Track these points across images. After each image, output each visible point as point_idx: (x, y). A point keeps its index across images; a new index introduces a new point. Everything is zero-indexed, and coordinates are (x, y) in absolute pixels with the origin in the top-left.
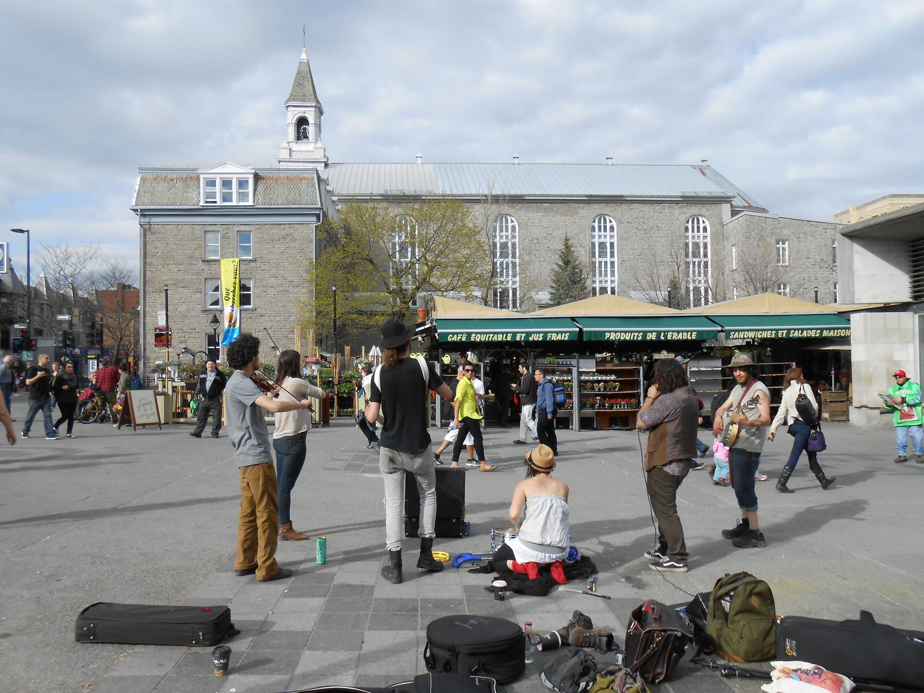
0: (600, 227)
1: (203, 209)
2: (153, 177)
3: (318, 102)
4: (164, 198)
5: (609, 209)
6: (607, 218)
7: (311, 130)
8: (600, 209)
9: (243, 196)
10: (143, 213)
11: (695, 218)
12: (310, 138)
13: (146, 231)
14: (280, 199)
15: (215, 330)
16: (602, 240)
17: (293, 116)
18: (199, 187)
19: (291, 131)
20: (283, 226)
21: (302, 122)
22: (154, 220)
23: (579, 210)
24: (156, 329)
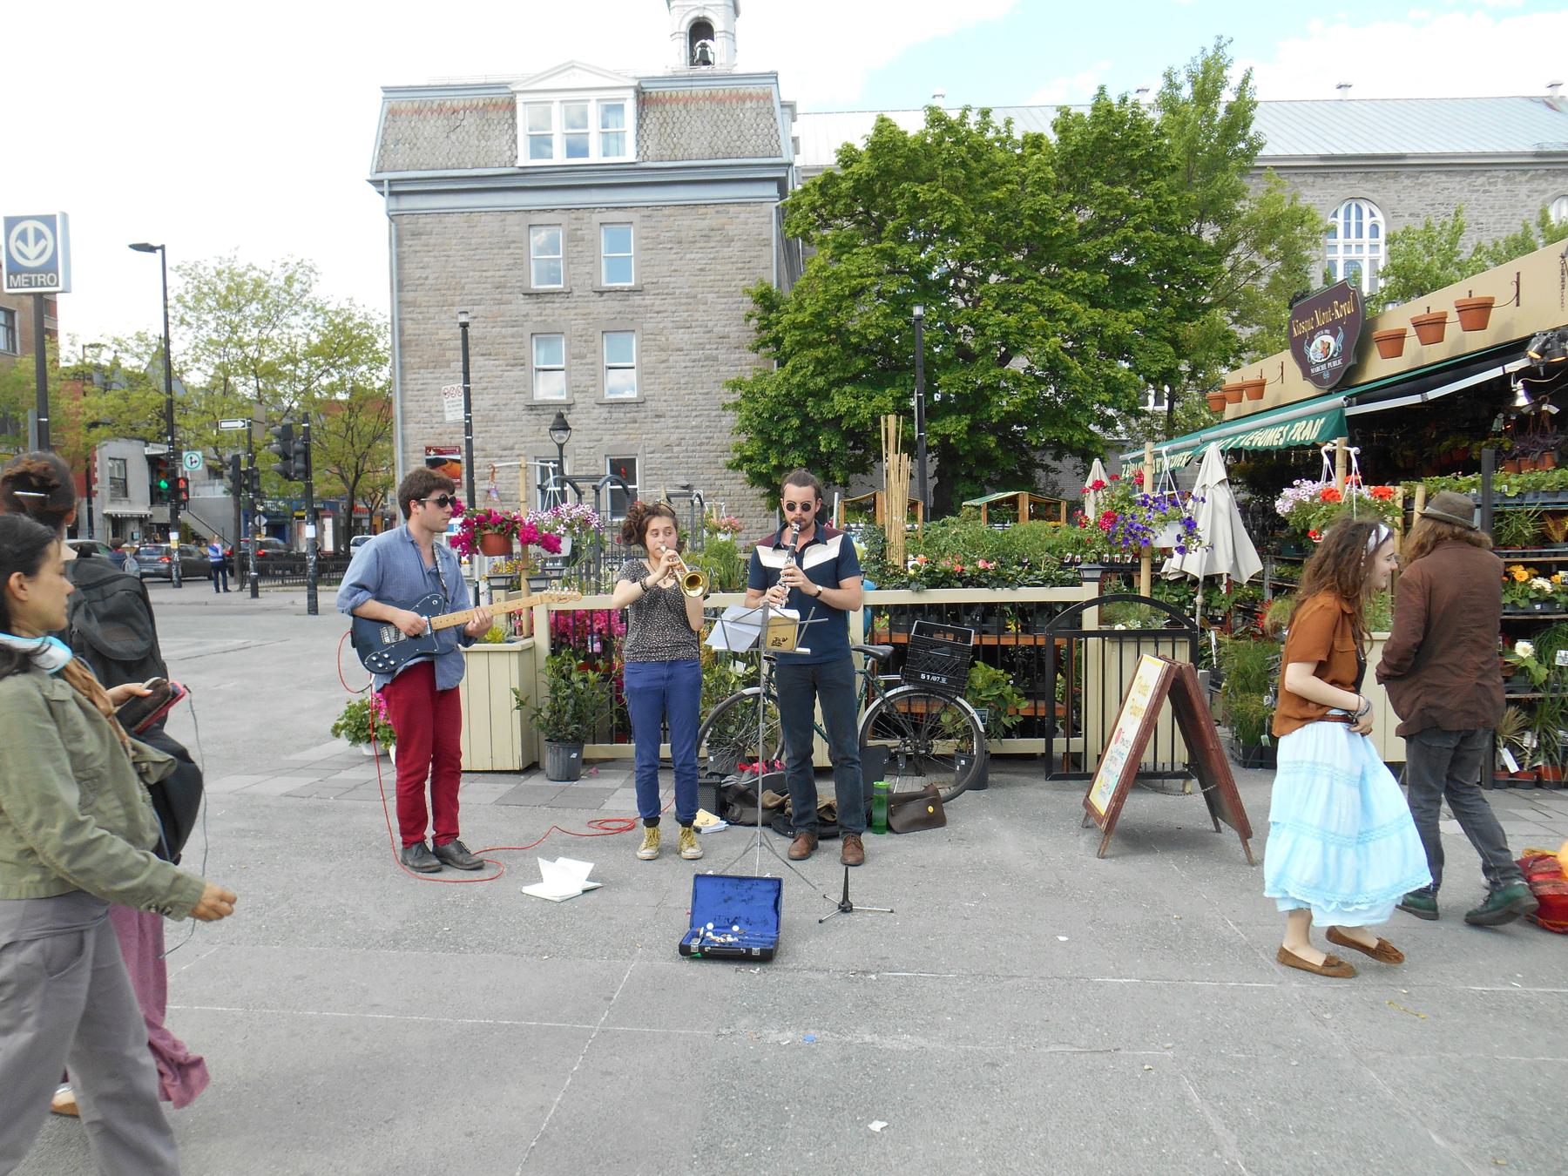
1: (526, 172)
4: (441, 153)
5: (1370, 186)
10: (395, 190)
13: (403, 233)
14: (697, 143)
15: (561, 447)
16: (1353, 255)
20: (702, 210)
24: (429, 448)
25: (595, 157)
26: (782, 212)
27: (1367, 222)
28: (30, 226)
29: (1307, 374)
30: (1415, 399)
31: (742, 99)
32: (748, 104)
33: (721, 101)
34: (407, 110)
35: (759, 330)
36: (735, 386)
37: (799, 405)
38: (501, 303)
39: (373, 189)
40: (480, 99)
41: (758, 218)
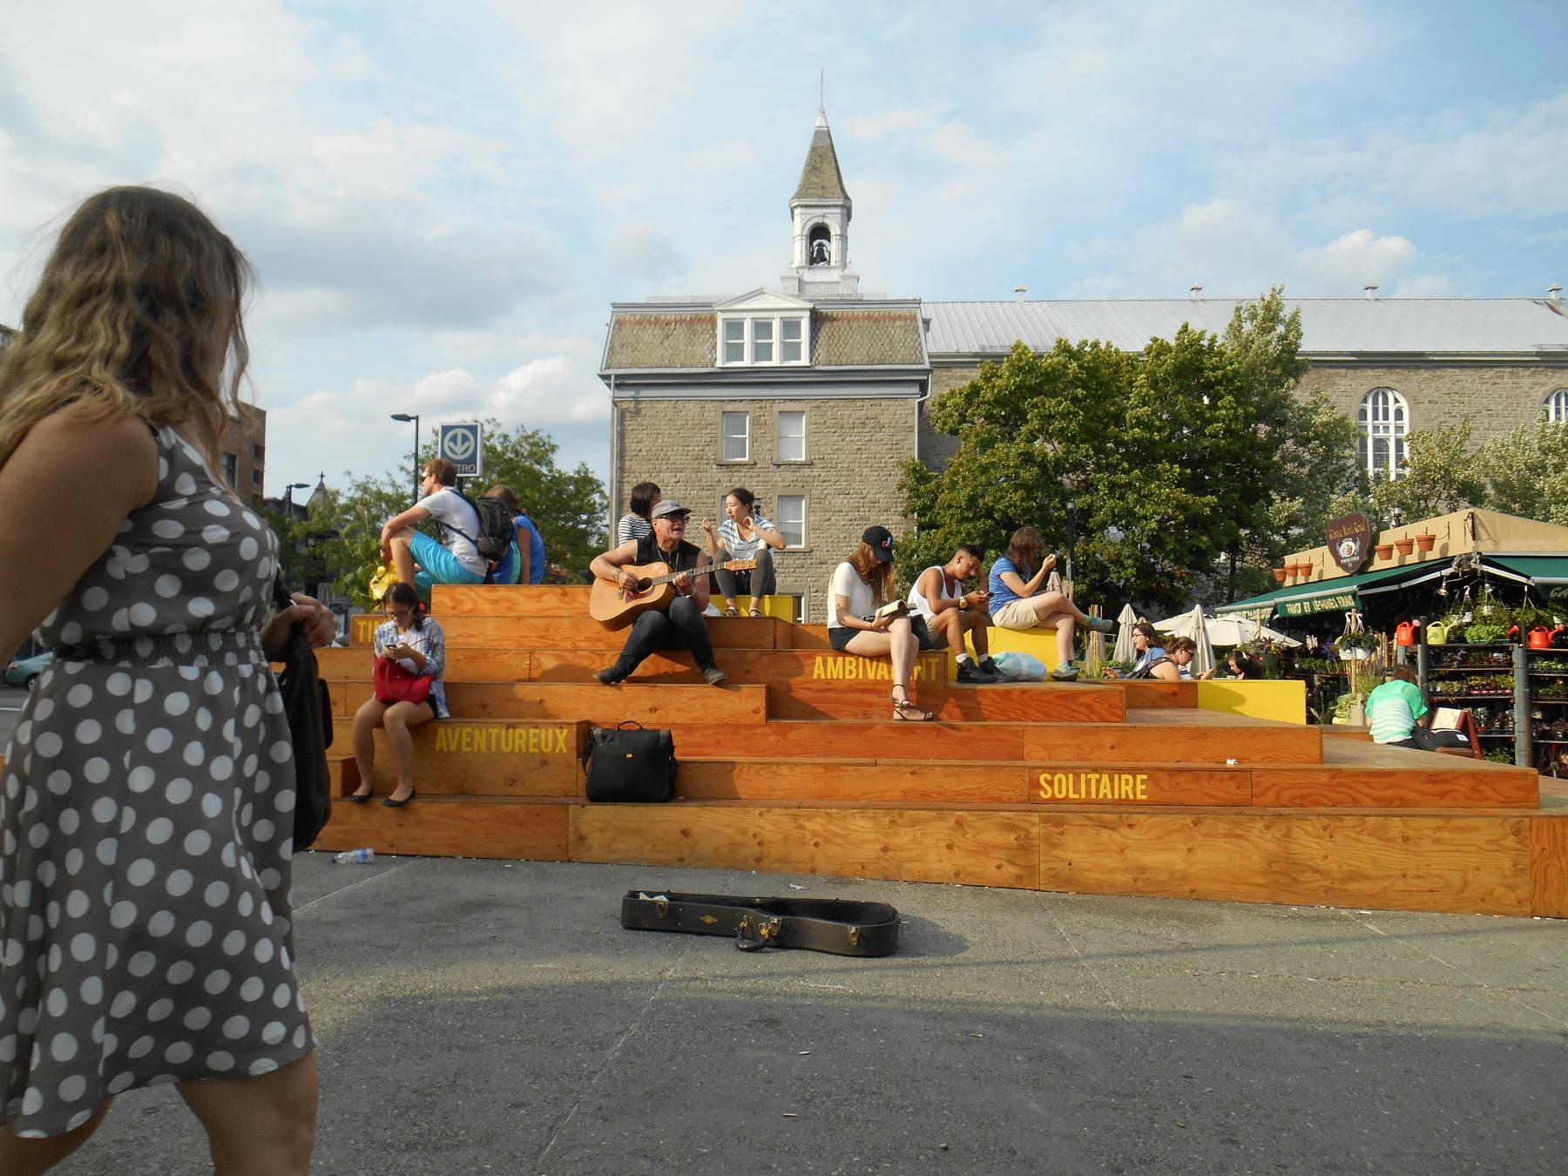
0: (1375, 411)
3: (846, 198)
4: (652, 357)
5: (1394, 377)
6: (1390, 395)
7: (833, 247)
8: (1378, 377)
9: (791, 350)
10: (621, 383)
11: (1380, 392)
13: (623, 417)
14: (856, 353)
16: (1381, 434)
17: (799, 226)
18: (714, 336)
19: (798, 251)
20: (859, 404)
21: (819, 232)
22: (644, 393)
23: (1337, 380)
25: (775, 361)
27: (1392, 408)
28: (459, 432)
29: (1338, 563)
30: (1395, 587)
31: (894, 319)
33: (877, 320)
34: (629, 321)
39: (602, 383)
40: (688, 314)
41: (900, 413)
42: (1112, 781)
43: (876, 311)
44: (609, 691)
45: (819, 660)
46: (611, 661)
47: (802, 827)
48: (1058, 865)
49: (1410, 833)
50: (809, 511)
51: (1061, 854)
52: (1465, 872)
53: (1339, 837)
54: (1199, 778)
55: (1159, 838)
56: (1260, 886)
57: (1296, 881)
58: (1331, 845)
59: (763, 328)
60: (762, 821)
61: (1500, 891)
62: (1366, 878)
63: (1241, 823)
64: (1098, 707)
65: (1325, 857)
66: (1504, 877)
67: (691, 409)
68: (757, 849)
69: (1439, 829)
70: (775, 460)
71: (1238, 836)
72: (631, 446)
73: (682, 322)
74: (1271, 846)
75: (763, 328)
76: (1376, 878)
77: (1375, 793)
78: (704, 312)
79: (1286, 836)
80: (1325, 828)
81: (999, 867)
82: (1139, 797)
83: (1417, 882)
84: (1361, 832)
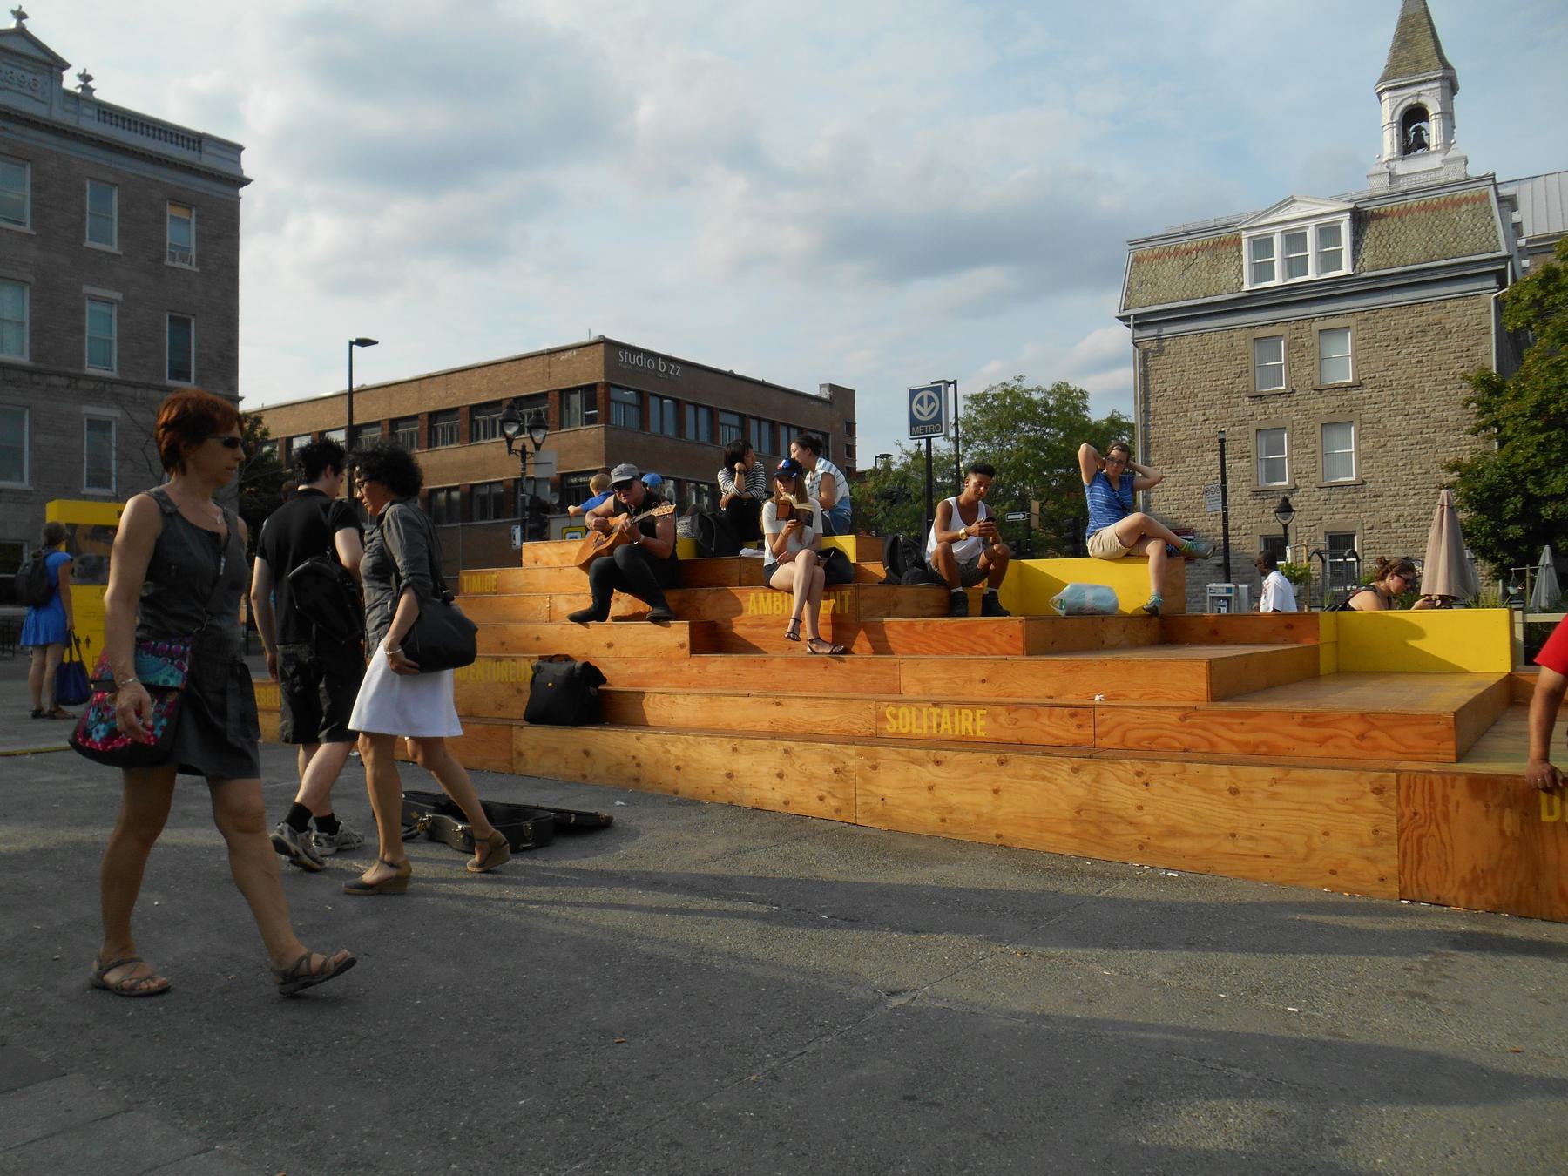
1: (1254, 295)
2: (1151, 253)
3: (1447, 66)
4: (1174, 289)
7: (1433, 129)
10: (1140, 322)
12: (1433, 143)
13: (1145, 359)
14: (1410, 249)
15: (1285, 526)
17: (1388, 111)
18: (1240, 258)
19: (1389, 142)
21: (1414, 116)
22: (1167, 330)
26: (1500, 304)
31: (1457, 203)
32: (1464, 207)
33: (1436, 208)
35: (1480, 415)
36: (1454, 467)
37: (1520, 485)
38: (1229, 405)
40: (1209, 238)
41: (1476, 315)
42: (952, 715)
43: (1434, 197)
44: (578, 628)
45: (752, 596)
46: (586, 603)
47: (668, 752)
48: (874, 800)
49: (1241, 785)
50: (1359, 438)
51: (874, 788)
52: (1309, 837)
53: (1156, 786)
54: (1038, 715)
55: (967, 776)
56: (1069, 835)
57: (1106, 832)
58: (1146, 794)
59: (1295, 240)
60: (639, 745)
61: (1356, 864)
62: (1186, 834)
63: (1047, 764)
64: (997, 639)
65: (1140, 808)
66: (1362, 846)
67: (1219, 341)
68: (635, 771)
69: (1275, 781)
70: (1317, 384)
71: (1044, 779)
72: (1155, 387)
73: (1204, 248)
74: (1080, 792)
75: (1295, 240)
76: (1199, 835)
77: (1237, 737)
78: (1227, 234)
79: (1095, 781)
80: (1139, 774)
81: (821, 799)
82: (979, 734)
83: (1249, 844)
84: (1181, 781)
